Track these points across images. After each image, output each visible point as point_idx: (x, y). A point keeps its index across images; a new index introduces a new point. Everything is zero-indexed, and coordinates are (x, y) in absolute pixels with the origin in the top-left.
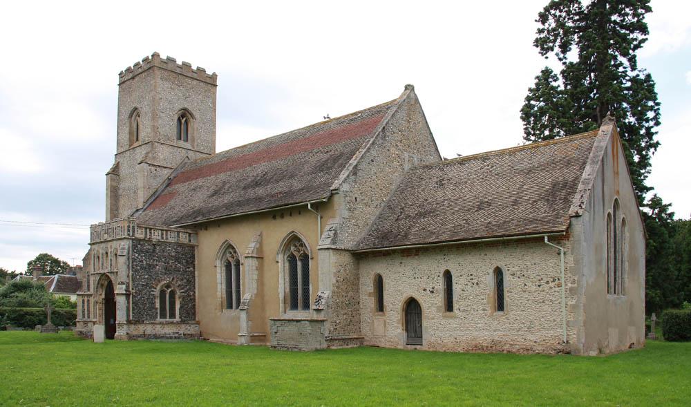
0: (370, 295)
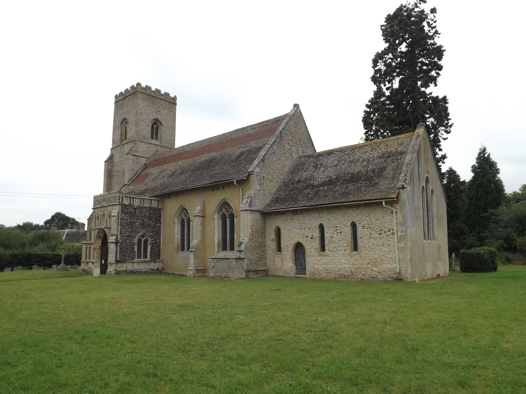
0: (272, 240)
